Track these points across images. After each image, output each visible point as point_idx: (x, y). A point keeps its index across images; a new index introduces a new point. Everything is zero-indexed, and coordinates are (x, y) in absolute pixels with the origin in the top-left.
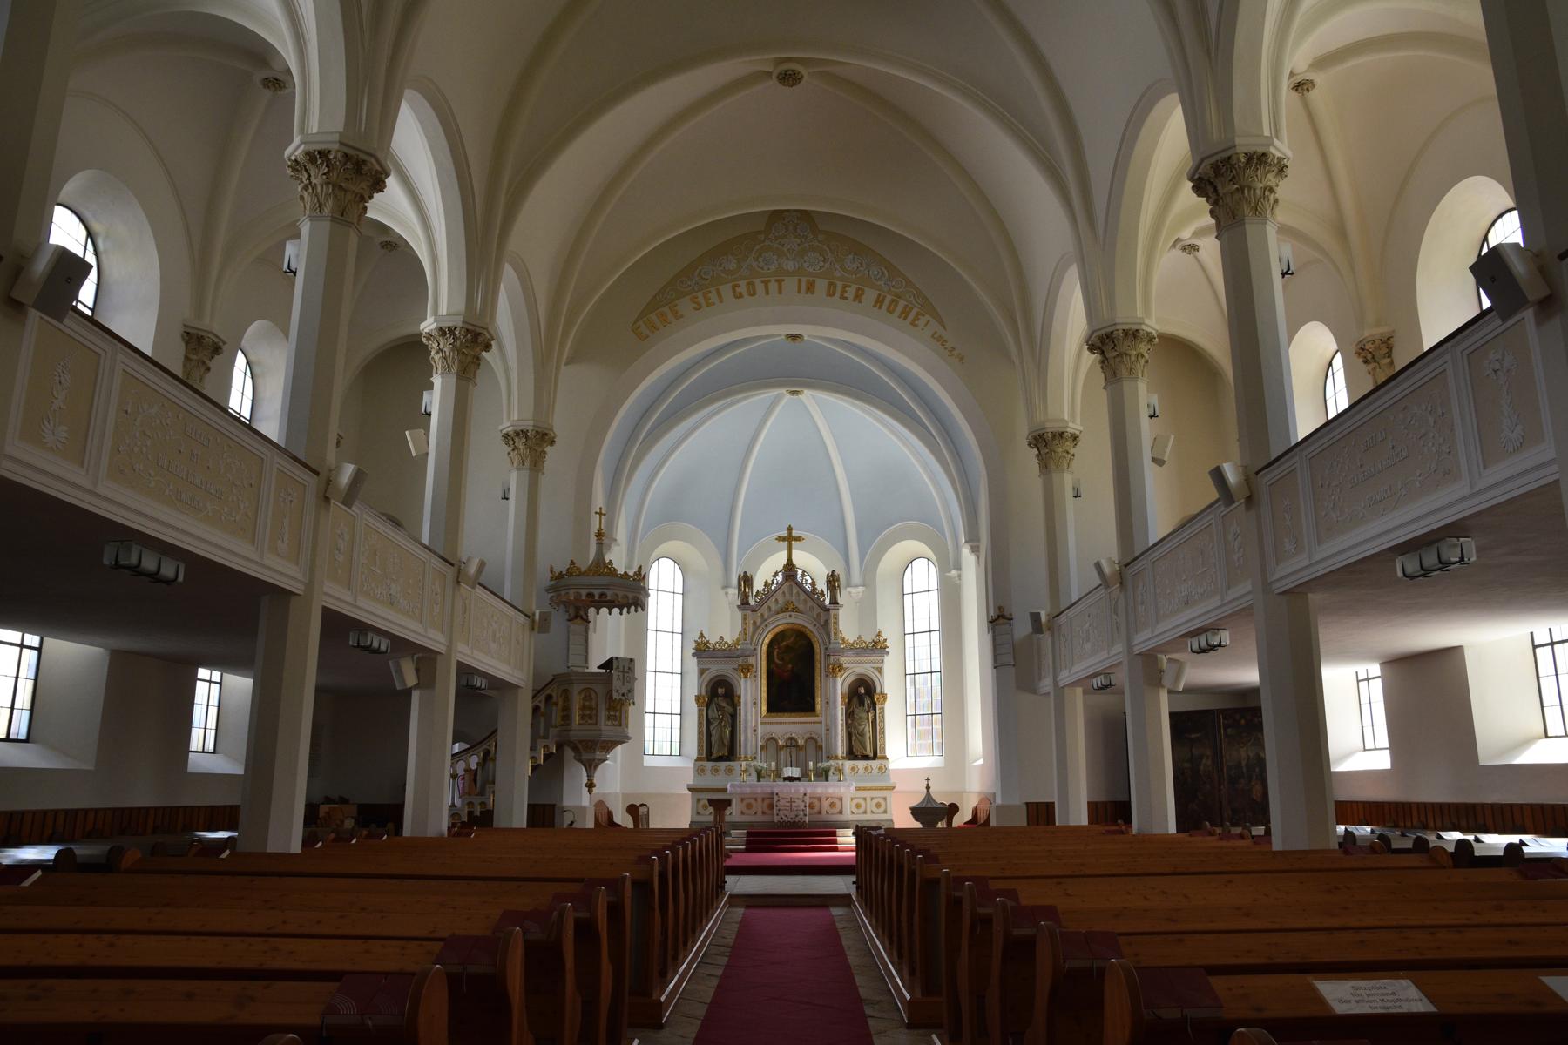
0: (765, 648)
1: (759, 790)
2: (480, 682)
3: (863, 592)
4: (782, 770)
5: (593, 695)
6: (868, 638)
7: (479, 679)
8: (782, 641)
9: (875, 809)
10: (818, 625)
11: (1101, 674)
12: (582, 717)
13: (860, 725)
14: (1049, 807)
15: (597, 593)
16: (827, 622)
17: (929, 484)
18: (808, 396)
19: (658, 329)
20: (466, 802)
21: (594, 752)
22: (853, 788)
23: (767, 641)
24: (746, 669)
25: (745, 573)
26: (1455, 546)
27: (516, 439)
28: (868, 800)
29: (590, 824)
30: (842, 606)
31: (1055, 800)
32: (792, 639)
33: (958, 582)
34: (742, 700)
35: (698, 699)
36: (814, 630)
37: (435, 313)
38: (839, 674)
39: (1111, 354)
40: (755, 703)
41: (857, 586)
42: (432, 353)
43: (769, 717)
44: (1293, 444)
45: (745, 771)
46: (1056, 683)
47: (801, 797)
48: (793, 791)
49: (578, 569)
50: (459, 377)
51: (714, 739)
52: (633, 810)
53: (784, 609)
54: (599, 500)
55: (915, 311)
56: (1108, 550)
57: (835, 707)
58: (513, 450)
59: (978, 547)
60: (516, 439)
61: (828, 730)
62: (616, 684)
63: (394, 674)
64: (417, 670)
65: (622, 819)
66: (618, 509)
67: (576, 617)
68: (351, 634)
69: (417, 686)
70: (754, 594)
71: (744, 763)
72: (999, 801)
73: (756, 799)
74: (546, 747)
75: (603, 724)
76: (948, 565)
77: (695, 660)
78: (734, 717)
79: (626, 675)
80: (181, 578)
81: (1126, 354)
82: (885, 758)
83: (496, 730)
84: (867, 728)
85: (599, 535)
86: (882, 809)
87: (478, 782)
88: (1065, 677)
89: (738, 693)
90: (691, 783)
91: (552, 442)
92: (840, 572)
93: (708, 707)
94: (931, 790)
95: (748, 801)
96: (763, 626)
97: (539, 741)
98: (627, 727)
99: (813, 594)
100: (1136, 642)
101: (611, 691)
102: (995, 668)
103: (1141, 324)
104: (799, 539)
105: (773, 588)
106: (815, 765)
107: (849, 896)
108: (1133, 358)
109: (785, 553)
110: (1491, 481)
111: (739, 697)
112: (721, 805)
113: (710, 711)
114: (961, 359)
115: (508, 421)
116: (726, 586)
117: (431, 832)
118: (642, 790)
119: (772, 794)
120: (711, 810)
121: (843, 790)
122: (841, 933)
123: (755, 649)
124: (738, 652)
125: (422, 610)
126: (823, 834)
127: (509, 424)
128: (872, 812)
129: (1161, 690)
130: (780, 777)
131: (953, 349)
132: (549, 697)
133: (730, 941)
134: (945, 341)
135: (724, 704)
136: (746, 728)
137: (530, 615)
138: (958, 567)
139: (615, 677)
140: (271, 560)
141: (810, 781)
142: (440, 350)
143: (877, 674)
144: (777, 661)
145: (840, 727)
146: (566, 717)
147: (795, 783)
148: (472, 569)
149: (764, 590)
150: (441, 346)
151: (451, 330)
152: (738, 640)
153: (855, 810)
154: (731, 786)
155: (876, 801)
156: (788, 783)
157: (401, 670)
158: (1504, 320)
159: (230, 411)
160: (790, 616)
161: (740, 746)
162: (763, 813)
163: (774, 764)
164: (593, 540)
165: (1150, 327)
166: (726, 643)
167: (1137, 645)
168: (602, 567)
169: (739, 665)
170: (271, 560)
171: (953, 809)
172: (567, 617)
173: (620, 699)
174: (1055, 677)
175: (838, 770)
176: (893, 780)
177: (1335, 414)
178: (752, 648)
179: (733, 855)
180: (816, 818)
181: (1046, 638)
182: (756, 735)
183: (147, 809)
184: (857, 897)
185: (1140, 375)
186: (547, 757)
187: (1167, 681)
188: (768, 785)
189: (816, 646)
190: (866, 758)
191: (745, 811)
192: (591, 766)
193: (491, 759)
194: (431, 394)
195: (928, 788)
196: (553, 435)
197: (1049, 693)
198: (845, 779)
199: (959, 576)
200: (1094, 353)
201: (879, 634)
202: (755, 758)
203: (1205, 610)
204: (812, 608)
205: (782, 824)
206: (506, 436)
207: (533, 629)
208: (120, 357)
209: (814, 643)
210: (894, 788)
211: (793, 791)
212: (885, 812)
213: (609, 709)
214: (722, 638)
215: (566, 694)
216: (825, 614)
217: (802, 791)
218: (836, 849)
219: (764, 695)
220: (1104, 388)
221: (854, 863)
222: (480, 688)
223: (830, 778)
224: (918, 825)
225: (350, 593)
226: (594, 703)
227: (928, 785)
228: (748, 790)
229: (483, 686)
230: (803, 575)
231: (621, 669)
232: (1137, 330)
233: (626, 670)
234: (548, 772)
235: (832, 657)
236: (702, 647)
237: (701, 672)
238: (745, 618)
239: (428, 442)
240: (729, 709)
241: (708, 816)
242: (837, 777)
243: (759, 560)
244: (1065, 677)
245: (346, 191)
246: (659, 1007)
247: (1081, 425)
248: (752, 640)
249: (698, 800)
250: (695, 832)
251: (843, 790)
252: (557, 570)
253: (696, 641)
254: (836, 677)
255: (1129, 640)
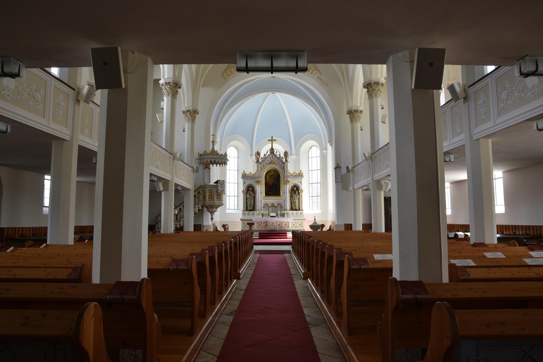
0: (264, 175)
1: (263, 220)
2: (180, 188)
3: (296, 157)
4: (270, 214)
5: (212, 192)
6: (297, 172)
7: (179, 187)
8: (270, 173)
9: (299, 226)
10: (281, 168)
11: (365, 186)
12: (209, 198)
13: (295, 200)
14: (351, 225)
15: (213, 160)
16: (284, 167)
17: (317, 122)
18: (277, 94)
19: (230, 76)
20: (175, 224)
21: (213, 209)
22: (292, 220)
23: (265, 173)
24: (258, 182)
25: (258, 151)
26: (448, 157)
27: (187, 113)
28: (297, 223)
29: (212, 230)
30: (289, 162)
31: (352, 223)
32: (273, 172)
33: (326, 154)
34: (257, 192)
35: (243, 191)
36: (280, 170)
37: (164, 78)
38: (288, 184)
39: (370, 89)
40: (261, 193)
41: (294, 155)
42: (163, 90)
43: (266, 197)
44: (485, 74)
45: (258, 214)
46: (353, 188)
47: (276, 222)
48: (273, 220)
49: (207, 153)
50: (172, 98)
51: (248, 204)
52: (224, 226)
53: (270, 163)
54: (212, 132)
55: (312, 69)
56: (368, 151)
57: (287, 194)
58: (186, 116)
59: (332, 144)
60: (187, 113)
61: (284, 201)
62: (219, 188)
63: (156, 187)
64: (163, 186)
65: (220, 229)
66: (217, 132)
67: (206, 167)
68: (93, 158)
69: (163, 190)
70: (261, 158)
71: (258, 212)
72: (336, 223)
73: (262, 223)
74: (198, 207)
75: (216, 200)
76: (323, 149)
77: (242, 179)
78: (254, 197)
79: (222, 185)
80: (9, 130)
81: (375, 89)
82: (302, 210)
83: (184, 202)
84: (297, 201)
85: (213, 142)
86: (301, 226)
87: (178, 218)
88: (356, 186)
89: (256, 190)
90: (241, 218)
91: (198, 113)
92: (288, 151)
93: (246, 194)
94: (316, 220)
95: (259, 224)
96: (264, 168)
97: (196, 206)
98: (223, 201)
99: (279, 158)
100: (475, 132)
101: (218, 190)
102: (336, 183)
103: (379, 80)
104: (275, 140)
105: (267, 156)
106: (280, 212)
107: (290, 251)
108: (377, 91)
109: (271, 144)
110: (454, 141)
111: (256, 191)
112: (251, 224)
113: (247, 195)
114: (327, 85)
115: (184, 107)
116: (251, 155)
117: (169, 232)
118: (226, 221)
119: (267, 221)
120: (248, 226)
121: (289, 220)
122: (287, 260)
123: (261, 176)
124: (256, 177)
125: (165, 168)
126: (283, 234)
127: (184, 108)
128: (298, 227)
129: (381, 191)
130: (269, 216)
131: (324, 82)
132: (199, 192)
133: (256, 261)
134: (322, 79)
135: (251, 193)
136: (258, 201)
137: (193, 167)
138: (326, 150)
139: (219, 186)
140: (53, 125)
141: (279, 217)
142: (166, 89)
143: (300, 183)
144: (268, 180)
145: (288, 200)
146: (204, 198)
147: (274, 218)
148: (178, 155)
149: (264, 157)
150: (166, 88)
151: (169, 83)
152: (256, 173)
153: (293, 226)
154: (254, 219)
155: (299, 224)
156: (271, 218)
157: (158, 186)
158: (455, 102)
159: (52, 73)
160: (272, 165)
161: (257, 206)
162: (264, 227)
163: (267, 212)
164: (211, 144)
165: (382, 81)
166: (252, 174)
167: (375, 177)
168: (214, 152)
169: (256, 181)
170: (53, 125)
171: (323, 226)
172: (203, 168)
173: (221, 193)
174: (353, 186)
175: (287, 214)
176: (305, 217)
177: (443, 105)
178: (260, 175)
179: (255, 240)
180: (281, 229)
181: (351, 174)
182: (262, 203)
183: (87, 226)
184: (292, 251)
185: (379, 96)
186: (198, 210)
187: (384, 188)
188: (265, 218)
189: (280, 173)
190: (296, 210)
191: (258, 226)
192: (212, 213)
193: (182, 211)
194: (164, 102)
195: (315, 219)
196: (180, 84)
197: (351, 191)
198: (290, 217)
199: (327, 152)
200: (365, 88)
201: (301, 171)
202: (261, 210)
203: (525, 111)
204: (279, 163)
205: (270, 230)
206: (184, 112)
207: (194, 172)
208: (53, 81)
209: (280, 174)
210: (305, 219)
211: (273, 220)
212: (302, 227)
213: (217, 196)
214: (250, 172)
215: (204, 192)
216: (283, 165)
217: (276, 220)
218: (287, 238)
219: (264, 190)
220: (368, 100)
221: (292, 242)
222: (179, 190)
223: (285, 216)
224: (312, 230)
225: (165, 173)
226: (213, 194)
227: (315, 218)
228: (259, 220)
229: (181, 190)
230: (276, 152)
231: (221, 184)
232: (378, 82)
233: (222, 184)
234: (199, 214)
235: (286, 178)
236: (244, 175)
237: (244, 183)
238: (258, 166)
239: (163, 117)
240: (253, 195)
241: (247, 228)
242: (287, 216)
243: (262, 147)
244: (356, 186)
245: (174, 90)
246: (239, 274)
247: (363, 108)
248: (260, 173)
249: (244, 223)
250: (243, 233)
251: (289, 220)
252: (200, 153)
253: (242, 173)
254: (287, 184)
255: (373, 176)
